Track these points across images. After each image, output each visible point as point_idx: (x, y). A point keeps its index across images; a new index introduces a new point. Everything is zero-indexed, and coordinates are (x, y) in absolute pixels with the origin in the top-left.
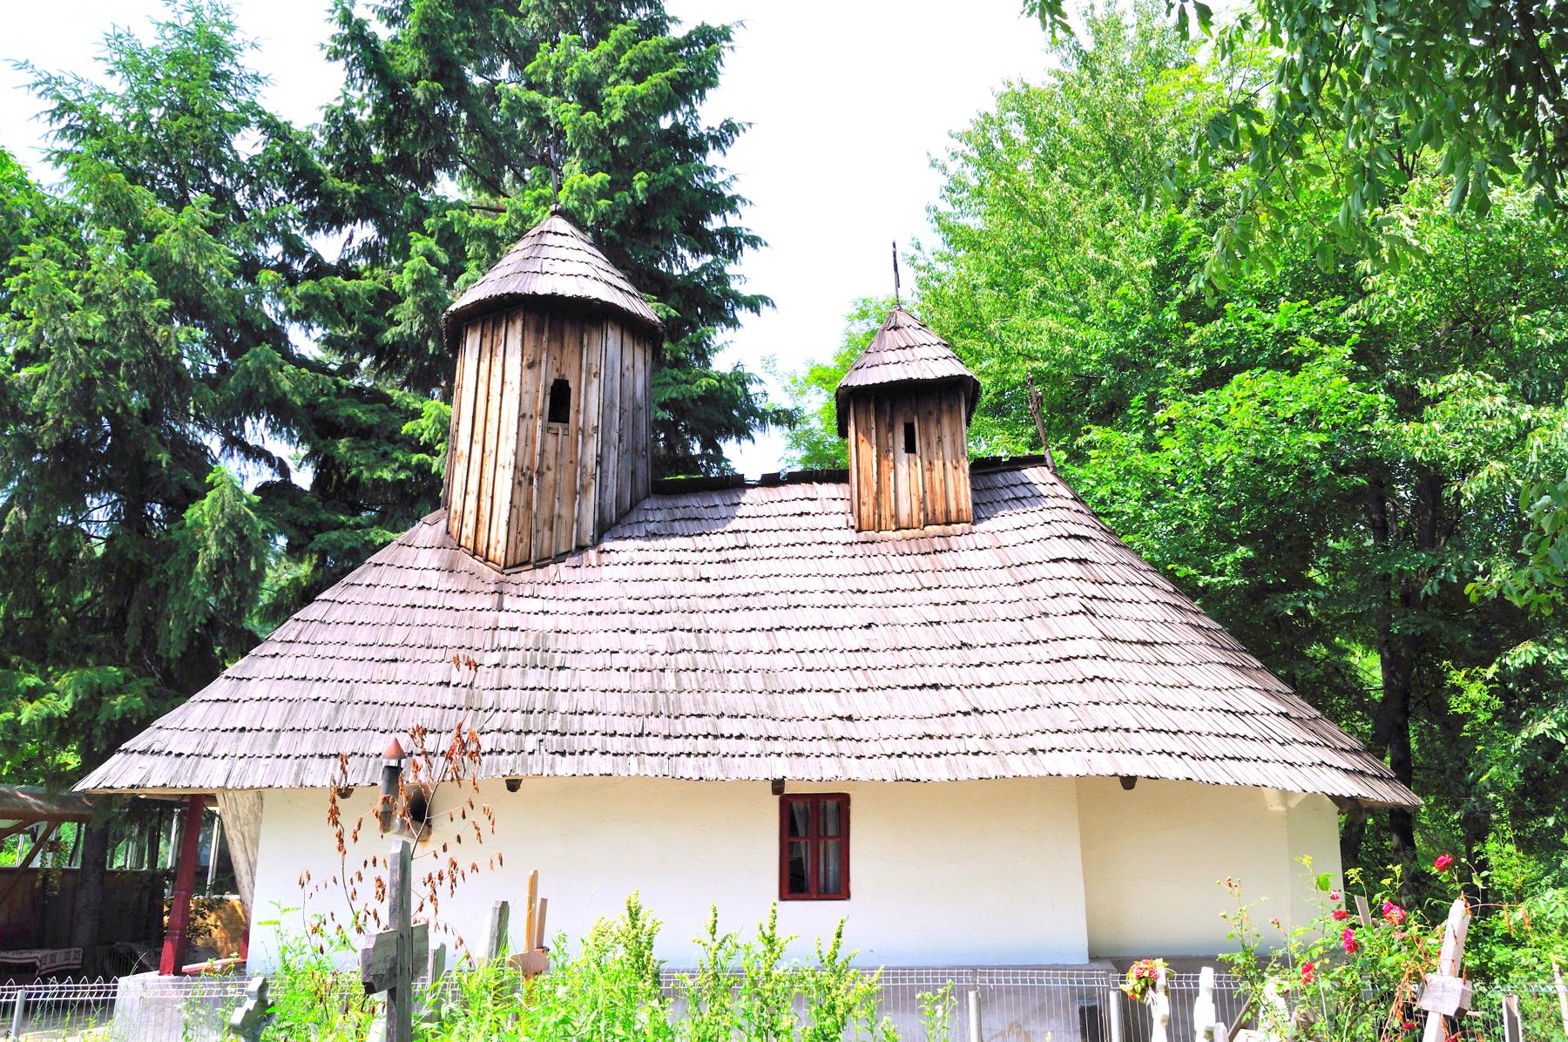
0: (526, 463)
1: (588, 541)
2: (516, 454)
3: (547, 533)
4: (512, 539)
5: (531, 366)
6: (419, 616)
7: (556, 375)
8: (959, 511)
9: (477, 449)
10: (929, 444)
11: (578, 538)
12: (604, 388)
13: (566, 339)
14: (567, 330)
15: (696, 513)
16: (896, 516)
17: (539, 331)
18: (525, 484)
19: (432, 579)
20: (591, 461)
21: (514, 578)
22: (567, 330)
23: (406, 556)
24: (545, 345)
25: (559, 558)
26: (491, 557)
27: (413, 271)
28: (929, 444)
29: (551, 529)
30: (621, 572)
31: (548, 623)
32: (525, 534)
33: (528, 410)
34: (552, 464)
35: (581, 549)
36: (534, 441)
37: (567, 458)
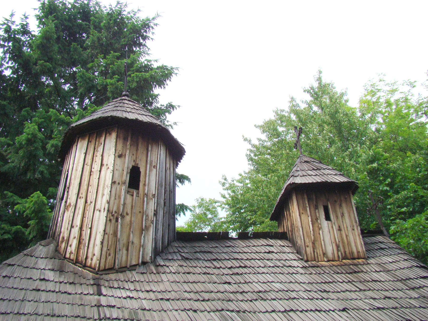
0: (115, 209)
1: (148, 259)
2: (108, 202)
3: (125, 252)
4: (104, 253)
5: (120, 156)
6: (44, 296)
7: (133, 164)
8: (358, 252)
9: (81, 202)
10: (337, 217)
11: (143, 257)
12: (158, 175)
13: (140, 145)
14: (140, 141)
17: (125, 140)
18: (113, 221)
19: (50, 275)
20: (151, 213)
21: (105, 277)
22: (140, 141)
23: (30, 261)
24: (128, 147)
25: (133, 268)
26: (89, 263)
27: (28, 134)
28: (337, 217)
29: (127, 250)
30: (171, 277)
31: (135, 304)
32: (112, 251)
33: (117, 179)
34: (129, 212)
36: (120, 197)
37: (137, 209)
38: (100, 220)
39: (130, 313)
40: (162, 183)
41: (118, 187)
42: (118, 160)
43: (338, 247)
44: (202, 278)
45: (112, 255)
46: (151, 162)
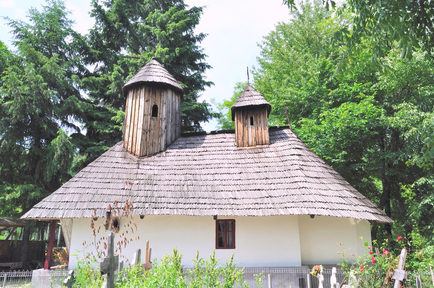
1: (163, 149)
2: (143, 126)
3: (151, 147)
5: (147, 101)
6: (116, 170)
7: (154, 104)
8: (265, 141)
9: (132, 124)
12: (167, 107)
15: (192, 142)
16: (248, 143)
17: (149, 92)
18: (145, 134)
19: (120, 160)
20: (163, 127)
21: (142, 160)
23: (112, 154)
24: (151, 95)
25: (155, 154)
26: (136, 154)
27: (114, 75)
28: (257, 123)
29: (153, 146)
30: (172, 158)
31: (151, 172)
32: (145, 148)
33: (146, 113)
34: (153, 128)
35: (161, 152)
36: (148, 122)
37: (157, 126)
38: (140, 132)
39: (149, 176)
40: (169, 111)
41: (147, 117)
42: (146, 103)
43: (255, 138)
44: (186, 158)
45: (146, 149)
46: (163, 101)
